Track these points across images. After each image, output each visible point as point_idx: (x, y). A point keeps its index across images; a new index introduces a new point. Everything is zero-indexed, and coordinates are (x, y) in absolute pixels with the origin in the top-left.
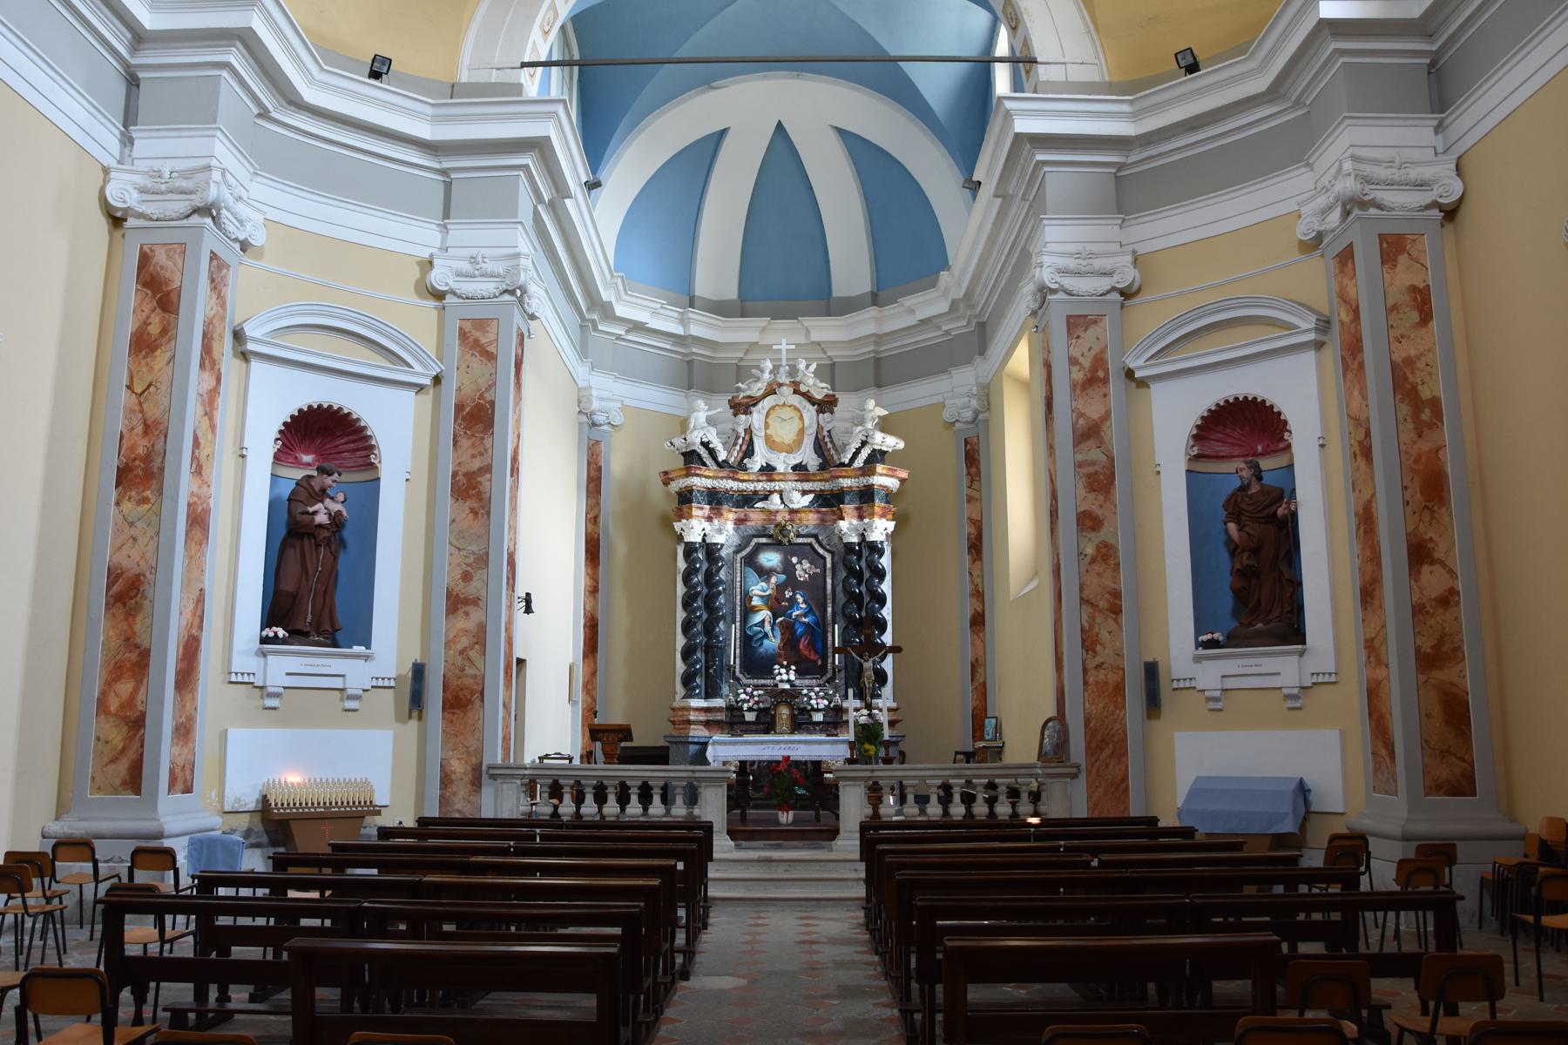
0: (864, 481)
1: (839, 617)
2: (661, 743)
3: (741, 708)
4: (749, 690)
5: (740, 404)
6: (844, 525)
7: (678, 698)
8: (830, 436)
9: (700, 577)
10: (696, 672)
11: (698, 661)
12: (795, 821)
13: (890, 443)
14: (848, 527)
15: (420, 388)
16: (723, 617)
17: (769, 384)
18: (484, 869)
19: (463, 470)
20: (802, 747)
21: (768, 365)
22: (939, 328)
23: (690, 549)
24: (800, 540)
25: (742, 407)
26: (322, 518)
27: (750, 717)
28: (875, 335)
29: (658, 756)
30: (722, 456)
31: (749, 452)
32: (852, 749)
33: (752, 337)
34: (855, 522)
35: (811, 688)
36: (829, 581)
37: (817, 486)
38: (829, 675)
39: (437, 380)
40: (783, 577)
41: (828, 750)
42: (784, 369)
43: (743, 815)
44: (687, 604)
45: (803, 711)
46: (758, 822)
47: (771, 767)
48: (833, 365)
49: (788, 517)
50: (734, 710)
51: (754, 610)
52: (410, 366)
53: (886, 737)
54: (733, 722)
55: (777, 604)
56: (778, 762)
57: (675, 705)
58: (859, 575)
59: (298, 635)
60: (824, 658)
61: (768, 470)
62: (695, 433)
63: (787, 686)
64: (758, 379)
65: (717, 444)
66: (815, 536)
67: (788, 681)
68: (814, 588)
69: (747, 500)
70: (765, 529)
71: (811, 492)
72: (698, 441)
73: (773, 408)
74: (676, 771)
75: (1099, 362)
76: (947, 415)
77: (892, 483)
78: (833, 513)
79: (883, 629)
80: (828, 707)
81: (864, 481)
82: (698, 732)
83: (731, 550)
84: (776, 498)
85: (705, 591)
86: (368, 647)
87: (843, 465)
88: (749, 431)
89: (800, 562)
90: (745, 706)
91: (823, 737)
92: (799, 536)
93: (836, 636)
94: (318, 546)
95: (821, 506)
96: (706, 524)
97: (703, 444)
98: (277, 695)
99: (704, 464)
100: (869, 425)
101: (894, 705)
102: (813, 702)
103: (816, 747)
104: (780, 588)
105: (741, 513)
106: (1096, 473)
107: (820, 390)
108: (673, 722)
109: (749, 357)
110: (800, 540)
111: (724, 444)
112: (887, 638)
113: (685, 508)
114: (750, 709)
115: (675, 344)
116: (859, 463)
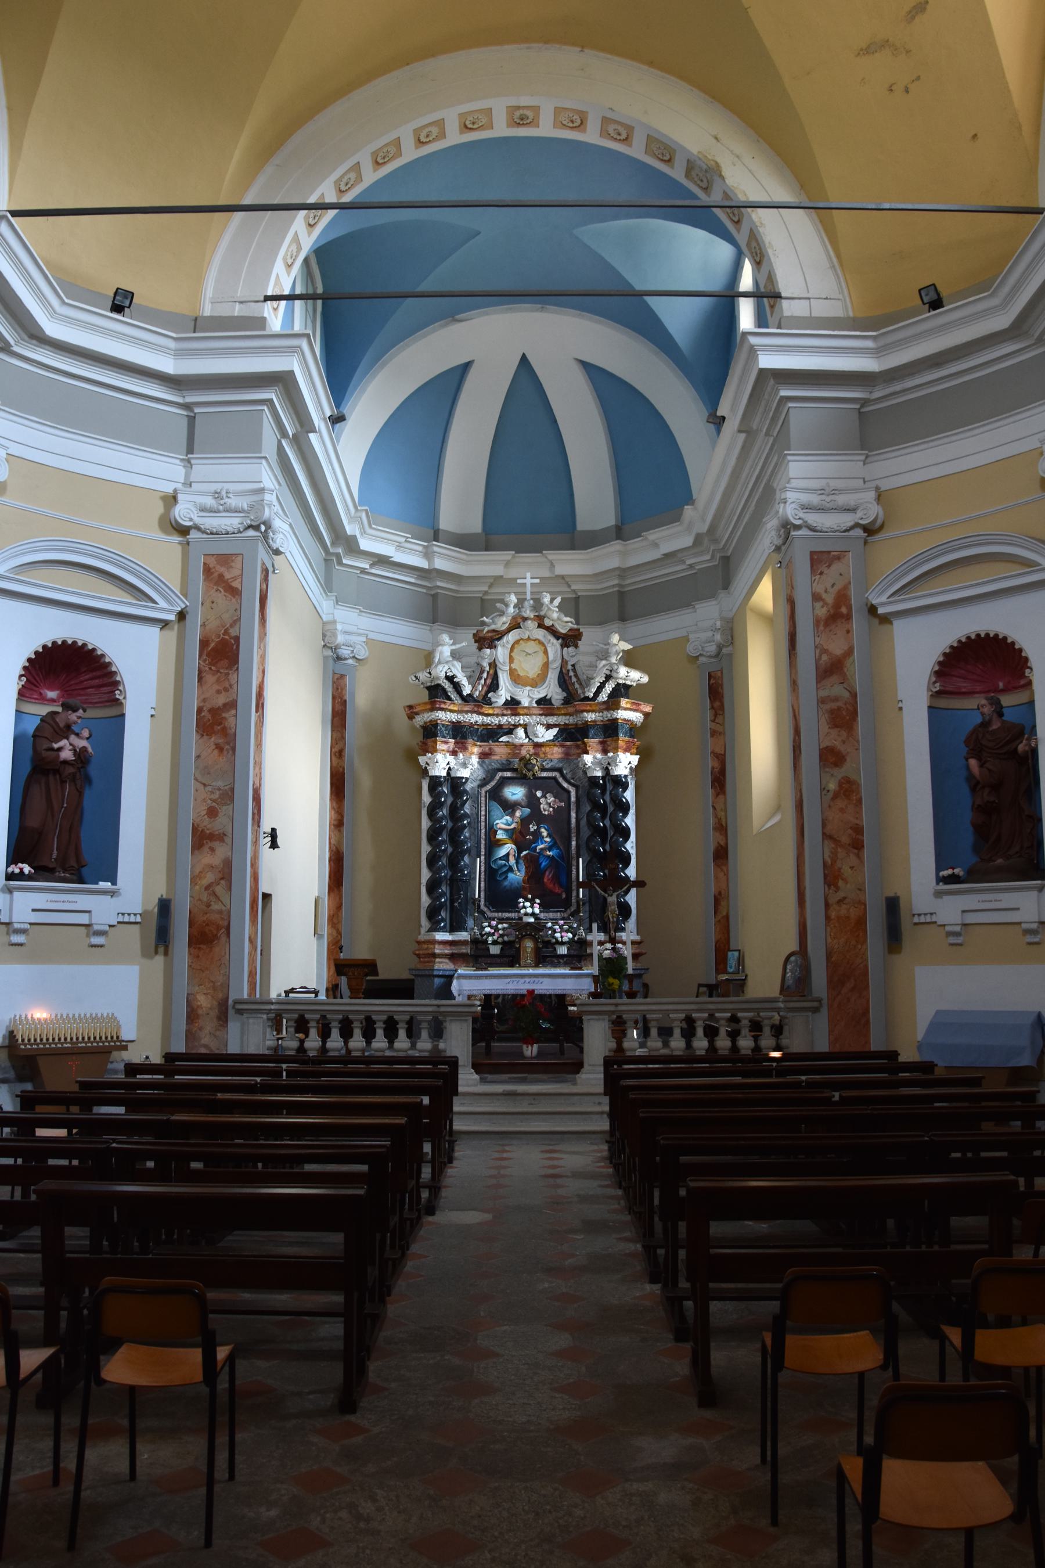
0: (608, 715)
1: (583, 851)
2: (405, 975)
3: (486, 941)
4: (494, 923)
6: (588, 759)
7: (423, 931)
8: (574, 670)
11: (443, 894)
12: (540, 1054)
13: (634, 677)
15: (165, 624)
16: (468, 851)
17: (514, 618)
19: (208, 706)
20: (546, 980)
21: (513, 599)
22: (683, 562)
23: (435, 783)
24: (545, 774)
25: (487, 641)
26: (67, 755)
27: (495, 950)
28: (618, 568)
29: (402, 989)
30: (467, 690)
31: (494, 686)
33: (498, 570)
34: (599, 756)
35: (555, 922)
36: (573, 815)
37: (562, 720)
39: (182, 616)
40: (528, 810)
43: (488, 1047)
44: (432, 837)
47: (515, 1000)
48: (577, 599)
49: (532, 751)
50: (479, 943)
51: (499, 844)
52: (155, 602)
53: (630, 971)
54: (478, 955)
55: (520, 837)
56: (523, 996)
57: (421, 938)
59: (43, 872)
61: (512, 705)
62: (440, 667)
63: (532, 920)
65: (462, 678)
66: (560, 770)
67: (533, 914)
68: (558, 822)
69: (491, 734)
70: (509, 762)
72: (443, 674)
73: (517, 642)
74: (421, 1005)
75: (842, 598)
76: (691, 649)
77: (636, 717)
78: (578, 747)
79: (627, 863)
81: (608, 715)
82: (443, 965)
83: (475, 784)
84: (520, 732)
85: (450, 825)
86: (114, 883)
87: (587, 699)
88: (493, 665)
90: (490, 939)
92: (543, 769)
94: (63, 782)
96: (450, 758)
97: (447, 678)
98: (23, 931)
99: (449, 698)
101: (638, 938)
102: (558, 935)
103: (560, 981)
104: (525, 821)
105: (486, 746)
106: (839, 708)
107: (564, 623)
108: (418, 956)
109: (493, 590)
110: (545, 774)
111: (469, 678)
112: (631, 872)
113: (430, 741)
114: (495, 943)
115: (420, 577)
116: (603, 697)
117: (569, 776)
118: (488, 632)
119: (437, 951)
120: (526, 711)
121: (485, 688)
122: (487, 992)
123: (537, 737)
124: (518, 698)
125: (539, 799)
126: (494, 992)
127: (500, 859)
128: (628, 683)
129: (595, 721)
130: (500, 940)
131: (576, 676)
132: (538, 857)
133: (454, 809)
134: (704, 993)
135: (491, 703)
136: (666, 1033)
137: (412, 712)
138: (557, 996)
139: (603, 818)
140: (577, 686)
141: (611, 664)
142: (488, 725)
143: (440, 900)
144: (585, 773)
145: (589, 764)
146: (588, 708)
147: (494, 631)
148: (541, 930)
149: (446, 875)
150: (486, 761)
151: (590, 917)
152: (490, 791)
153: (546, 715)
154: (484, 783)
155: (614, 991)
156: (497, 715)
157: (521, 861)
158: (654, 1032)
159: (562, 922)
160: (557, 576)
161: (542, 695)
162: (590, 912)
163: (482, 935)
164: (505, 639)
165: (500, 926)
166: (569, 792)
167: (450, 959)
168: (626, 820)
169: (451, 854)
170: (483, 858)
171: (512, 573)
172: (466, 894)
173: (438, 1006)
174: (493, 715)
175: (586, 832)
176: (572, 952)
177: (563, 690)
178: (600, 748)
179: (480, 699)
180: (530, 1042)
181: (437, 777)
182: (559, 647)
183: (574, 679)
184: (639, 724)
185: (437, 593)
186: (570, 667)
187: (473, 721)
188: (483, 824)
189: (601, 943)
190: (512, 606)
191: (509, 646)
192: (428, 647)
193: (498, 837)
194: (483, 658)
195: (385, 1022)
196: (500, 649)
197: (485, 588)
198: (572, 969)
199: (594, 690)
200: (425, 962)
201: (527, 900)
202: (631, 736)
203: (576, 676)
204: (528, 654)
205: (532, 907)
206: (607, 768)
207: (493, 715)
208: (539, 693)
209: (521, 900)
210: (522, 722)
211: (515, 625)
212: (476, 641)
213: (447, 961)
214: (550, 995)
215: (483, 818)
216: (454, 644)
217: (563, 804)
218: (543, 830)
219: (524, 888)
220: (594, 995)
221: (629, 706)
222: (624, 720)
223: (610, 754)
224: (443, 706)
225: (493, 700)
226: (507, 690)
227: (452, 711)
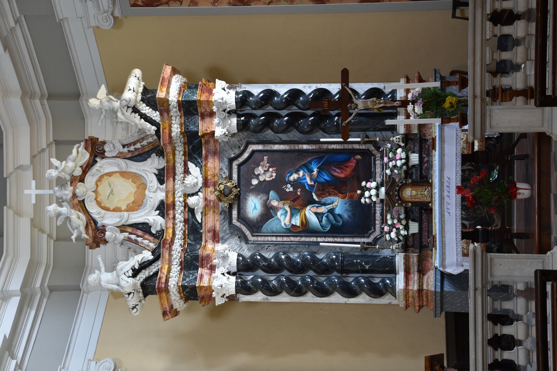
0: (174, 111)
1: (313, 137)
2: (442, 320)
4: (386, 229)
5: (95, 238)
6: (219, 132)
7: (395, 302)
8: (129, 145)
9: (272, 278)
10: (369, 282)
11: (357, 280)
12: (527, 180)
13: (134, 84)
14: (221, 128)
16: (313, 254)
17: (74, 207)
20: (446, 174)
21: (53, 208)
22: (12, 30)
23: (243, 288)
24: (235, 176)
25: (97, 235)
27: (414, 228)
28: (23, 99)
29: (457, 326)
30: (148, 255)
31: (145, 228)
32: (449, 121)
33: (25, 225)
34: (216, 120)
35: (384, 166)
36: (276, 147)
37: (180, 158)
38: (372, 148)
40: (272, 193)
41: (450, 145)
42: (57, 192)
43: (519, 236)
44: (298, 291)
45: (408, 174)
46: (528, 219)
47: (469, 207)
48: (57, 142)
49: (211, 189)
50: (407, 244)
51: (305, 223)
53: (438, 84)
54: (420, 246)
55: (300, 200)
56: (463, 199)
57: (402, 304)
58: (271, 117)
60: (354, 152)
61: (163, 208)
62: (123, 283)
63: (383, 190)
64: (68, 219)
65: (135, 261)
66: (231, 161)
67: (377, 188)
68: (283, 162)
69: (194, 230)
70: (222, 212)
71: (186, 165)
72: (131, 280)
73: (99, 204)
74: (476, 307)
76: (107, 25)
77: (176, 82)
78: (207, 142)
79: (325, 92)
80: (403, 148)
81: (174, 111)
82: (431, 282)
83: (245, 246)
84: (192, 201)
85: (286, 273)
87: (157, 132)
88: (122, 228)
89: (257, 177)
90: (403, 232)
91: (436, 155)
92: (230, 177)
93: (331, 141)
95: (200, 155)
96: (218, 272)
97: (134, 275)
99: (156, 274)
100: (116, 104)
101: (403, 81)
102: (399, 163)
103: (447, 160)
104: (283, 196)
105: (207, 236)
107: (80, 155)
108: (421, 307)
109: (47, 228)
110: (235, 176)
111: (136, 253)
112: (334, 88)
113: (200, 293)
114: (406, 227)
115: (30, 305)
116: (155, 115)
117: (237, 152)
118: (87, 233)
119: (416, 287)
120: (170, 195)
121: (147, 236)
122: (459, 235)
124: (157, 203)
125: (260, 182)
126: (459, 229)
127: (320, 221)
128: (141, 89)
129: (181, 125)
130: (404, 222)
131: (134, 143)
132: (319, 183)
133: (270, 268)
134: (462, 12)
135: (162, 231)
136: (505, 43)
137: (170, 312)
138: (463, 163)
139: (279, 116)
140: (145, 143)
141: (122, 107)
142: (184, 234)
143: (363, 284)
144: (233, 135)
145: (225, 130)
146: (167, 131)
147: (87, 227)
148: (394, 180)
149: (338, 278)
150: (221, 235)
151: (381, 130)
152: (252, 232)
153: (174, 174)
154: (243, 238)
155: (459, 102)
156: (174, 224)
157: (323, 200)
158: (506, 56)
159: (386, 159)
160: (32, 162)
161: (154, 179)
162: (375, 130)
163: (399, 241)
164: (95, 216)
165: (390, 222)
166: (253, 152)
167: (424, 275)
168: (282, 93)
169: (315, 271)
170: (319, 239)
171: (29, 210)
172: (357, 257)
173: (476, 289)
174: (174, 228)
175: (294, 134)
176: (417, 148)
177: (149, 156)
178: (207, 120)
179: (157, 241)
180: (512, 191)
181: (236, 286)
182: (104, 161)
183: (138, 146)
184: (185, 80)
185: (48, 286)
186: (126, 150)
187: (180, 249)
188: (285, 239)
189: (408, 116)
190: (60, 209)
191: (103, 212)
192: (106, 295)
193: (298, 224)
194: (115, 239)
195: (495, 349)
196: (106, 222)
197: (45, 236)
198: (434, 148)
199: (148, 125)
200: (427, 300)
201: (362, 195)
202: (196, 87)
203: (134, 143)
204: (112, 192)
205: (369, 189)
206: (229, 112)
207: (174, 228)
208: (153, 181)
209: (363, 200)
210: (182, 199)
211: (81, 206)
212: (98, 246)
213: (425, 278)
214: (463, 171)
215: (279, 239)
216: (99, 269)
217: (266, 158)
218: (291, 178)
219: (351, 197)
220: (463, 121)
221: (165, 89)
222: (179, 94)
223: (215, 109)
224: (163, 280)
225: (159, 228)
226: (149, 213)
227: (169, 271)
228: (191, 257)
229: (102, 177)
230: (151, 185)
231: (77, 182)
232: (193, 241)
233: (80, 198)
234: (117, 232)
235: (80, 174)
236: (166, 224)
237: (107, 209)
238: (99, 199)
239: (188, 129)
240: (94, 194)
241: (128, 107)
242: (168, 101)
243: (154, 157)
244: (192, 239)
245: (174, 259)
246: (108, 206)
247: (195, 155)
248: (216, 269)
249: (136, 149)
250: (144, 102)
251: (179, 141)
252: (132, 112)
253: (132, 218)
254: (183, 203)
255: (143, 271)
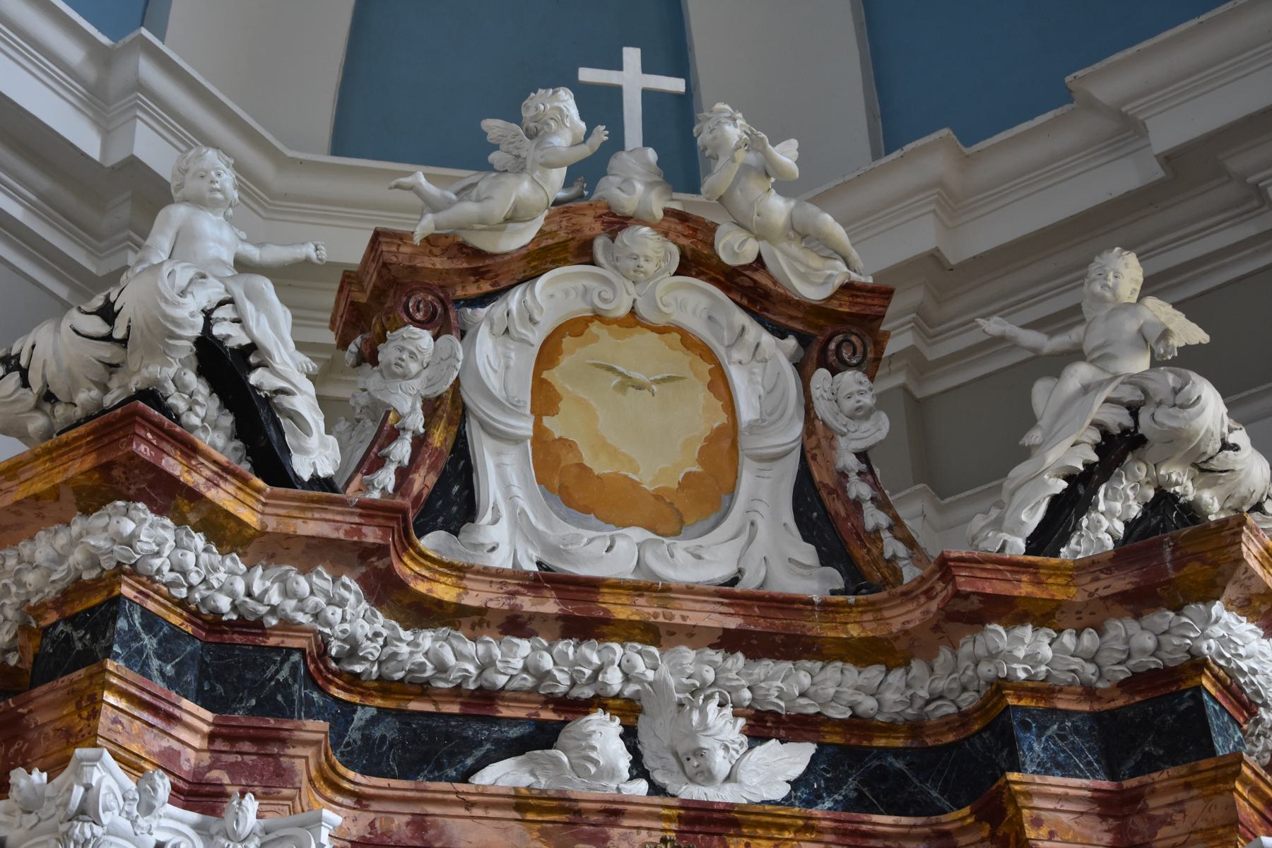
0: (1139, 640)
18: (1232, 218)
37: (835, 688)
72: (188, 314)
73: (574, 327)
81: (1139, 640)
88: (450, 408)
115: (46, 206)
123: (705, 775)
129: (1043, 690)
186: (849, 461)
191: (537, 337)
196: (486, 347)
199: (1032, 518)
204: (628, 383)
228: (284, 686)
229: (706, 353)
230: (680, 554)
231: (685, 242)
232: (366, 738)
233: (606, 249)
234: (430, 382)
235: (724, 257)
236: (486, 572)
237: (548, 353)
238: (595, 328)
239: (1026, 727)
240: (623, 311)
241: (1134, 410)
242: (1209, 594)
243: (823, 578)
244: (377, 733)
245: (282, 580)
246: (565, 361)
247: (852, 782)
248: (194, 816)
249: (857, 504)
250: (1149, 508)
251: (941, 685)
252: (1105, 434)
253: (499, 454)
254: (588, 693)
255: (228, 420)
